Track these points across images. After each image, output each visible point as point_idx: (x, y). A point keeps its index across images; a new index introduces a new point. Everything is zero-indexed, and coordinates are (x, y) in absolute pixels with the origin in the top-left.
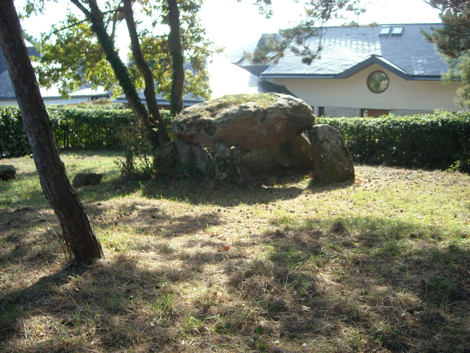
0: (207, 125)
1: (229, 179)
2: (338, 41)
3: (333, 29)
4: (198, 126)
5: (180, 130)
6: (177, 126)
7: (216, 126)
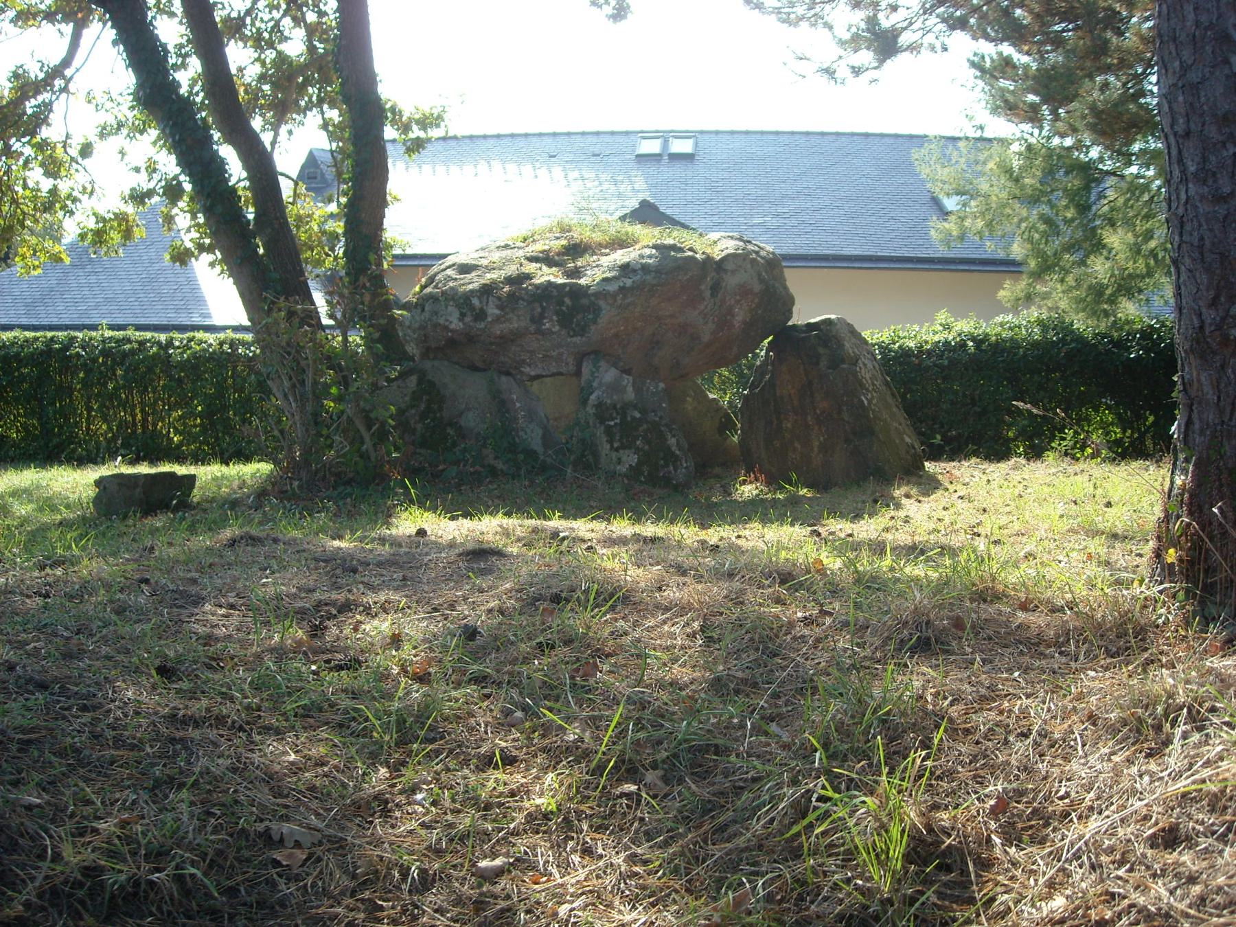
0: (567, 301)
1: (645, 469)
2: (527, 169)
3: (521, 143)
4: (537, 305)
5: (468, 319)
6: (458, 306)
7: (601, 303)
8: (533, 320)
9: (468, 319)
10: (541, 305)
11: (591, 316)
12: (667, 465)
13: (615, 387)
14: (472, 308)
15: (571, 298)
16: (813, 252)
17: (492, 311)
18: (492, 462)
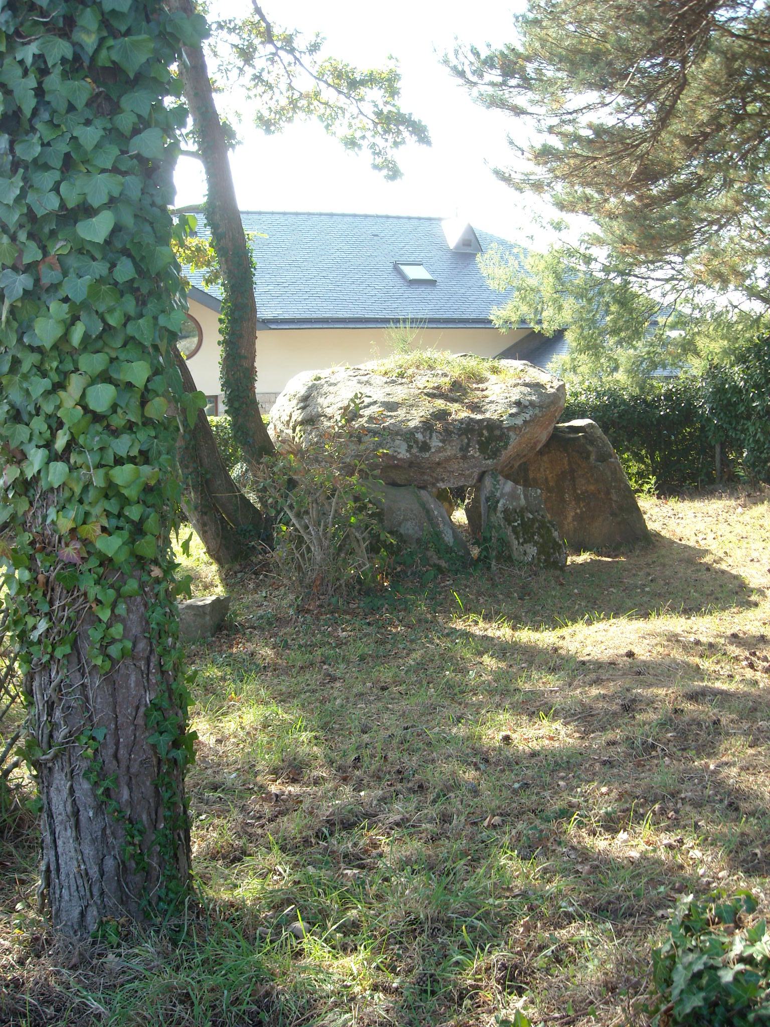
0: (485, 433)
4: (464, 437)
5: (415, 450)
6: (406, 440)
8: (461, 449)
9: (415, 450)
10: (468, 438)
11: (502, 444)
12: (555, 553)
13: (513, 496)
14: (416, 442)
15: (488, 431)
16: (314, 316)
17: (435, 443)
18: (437, 562)
